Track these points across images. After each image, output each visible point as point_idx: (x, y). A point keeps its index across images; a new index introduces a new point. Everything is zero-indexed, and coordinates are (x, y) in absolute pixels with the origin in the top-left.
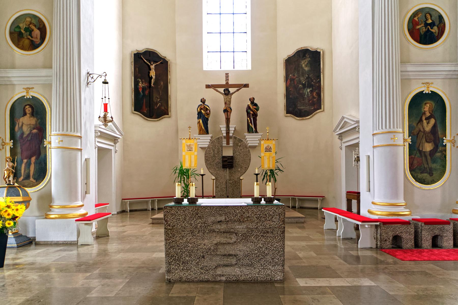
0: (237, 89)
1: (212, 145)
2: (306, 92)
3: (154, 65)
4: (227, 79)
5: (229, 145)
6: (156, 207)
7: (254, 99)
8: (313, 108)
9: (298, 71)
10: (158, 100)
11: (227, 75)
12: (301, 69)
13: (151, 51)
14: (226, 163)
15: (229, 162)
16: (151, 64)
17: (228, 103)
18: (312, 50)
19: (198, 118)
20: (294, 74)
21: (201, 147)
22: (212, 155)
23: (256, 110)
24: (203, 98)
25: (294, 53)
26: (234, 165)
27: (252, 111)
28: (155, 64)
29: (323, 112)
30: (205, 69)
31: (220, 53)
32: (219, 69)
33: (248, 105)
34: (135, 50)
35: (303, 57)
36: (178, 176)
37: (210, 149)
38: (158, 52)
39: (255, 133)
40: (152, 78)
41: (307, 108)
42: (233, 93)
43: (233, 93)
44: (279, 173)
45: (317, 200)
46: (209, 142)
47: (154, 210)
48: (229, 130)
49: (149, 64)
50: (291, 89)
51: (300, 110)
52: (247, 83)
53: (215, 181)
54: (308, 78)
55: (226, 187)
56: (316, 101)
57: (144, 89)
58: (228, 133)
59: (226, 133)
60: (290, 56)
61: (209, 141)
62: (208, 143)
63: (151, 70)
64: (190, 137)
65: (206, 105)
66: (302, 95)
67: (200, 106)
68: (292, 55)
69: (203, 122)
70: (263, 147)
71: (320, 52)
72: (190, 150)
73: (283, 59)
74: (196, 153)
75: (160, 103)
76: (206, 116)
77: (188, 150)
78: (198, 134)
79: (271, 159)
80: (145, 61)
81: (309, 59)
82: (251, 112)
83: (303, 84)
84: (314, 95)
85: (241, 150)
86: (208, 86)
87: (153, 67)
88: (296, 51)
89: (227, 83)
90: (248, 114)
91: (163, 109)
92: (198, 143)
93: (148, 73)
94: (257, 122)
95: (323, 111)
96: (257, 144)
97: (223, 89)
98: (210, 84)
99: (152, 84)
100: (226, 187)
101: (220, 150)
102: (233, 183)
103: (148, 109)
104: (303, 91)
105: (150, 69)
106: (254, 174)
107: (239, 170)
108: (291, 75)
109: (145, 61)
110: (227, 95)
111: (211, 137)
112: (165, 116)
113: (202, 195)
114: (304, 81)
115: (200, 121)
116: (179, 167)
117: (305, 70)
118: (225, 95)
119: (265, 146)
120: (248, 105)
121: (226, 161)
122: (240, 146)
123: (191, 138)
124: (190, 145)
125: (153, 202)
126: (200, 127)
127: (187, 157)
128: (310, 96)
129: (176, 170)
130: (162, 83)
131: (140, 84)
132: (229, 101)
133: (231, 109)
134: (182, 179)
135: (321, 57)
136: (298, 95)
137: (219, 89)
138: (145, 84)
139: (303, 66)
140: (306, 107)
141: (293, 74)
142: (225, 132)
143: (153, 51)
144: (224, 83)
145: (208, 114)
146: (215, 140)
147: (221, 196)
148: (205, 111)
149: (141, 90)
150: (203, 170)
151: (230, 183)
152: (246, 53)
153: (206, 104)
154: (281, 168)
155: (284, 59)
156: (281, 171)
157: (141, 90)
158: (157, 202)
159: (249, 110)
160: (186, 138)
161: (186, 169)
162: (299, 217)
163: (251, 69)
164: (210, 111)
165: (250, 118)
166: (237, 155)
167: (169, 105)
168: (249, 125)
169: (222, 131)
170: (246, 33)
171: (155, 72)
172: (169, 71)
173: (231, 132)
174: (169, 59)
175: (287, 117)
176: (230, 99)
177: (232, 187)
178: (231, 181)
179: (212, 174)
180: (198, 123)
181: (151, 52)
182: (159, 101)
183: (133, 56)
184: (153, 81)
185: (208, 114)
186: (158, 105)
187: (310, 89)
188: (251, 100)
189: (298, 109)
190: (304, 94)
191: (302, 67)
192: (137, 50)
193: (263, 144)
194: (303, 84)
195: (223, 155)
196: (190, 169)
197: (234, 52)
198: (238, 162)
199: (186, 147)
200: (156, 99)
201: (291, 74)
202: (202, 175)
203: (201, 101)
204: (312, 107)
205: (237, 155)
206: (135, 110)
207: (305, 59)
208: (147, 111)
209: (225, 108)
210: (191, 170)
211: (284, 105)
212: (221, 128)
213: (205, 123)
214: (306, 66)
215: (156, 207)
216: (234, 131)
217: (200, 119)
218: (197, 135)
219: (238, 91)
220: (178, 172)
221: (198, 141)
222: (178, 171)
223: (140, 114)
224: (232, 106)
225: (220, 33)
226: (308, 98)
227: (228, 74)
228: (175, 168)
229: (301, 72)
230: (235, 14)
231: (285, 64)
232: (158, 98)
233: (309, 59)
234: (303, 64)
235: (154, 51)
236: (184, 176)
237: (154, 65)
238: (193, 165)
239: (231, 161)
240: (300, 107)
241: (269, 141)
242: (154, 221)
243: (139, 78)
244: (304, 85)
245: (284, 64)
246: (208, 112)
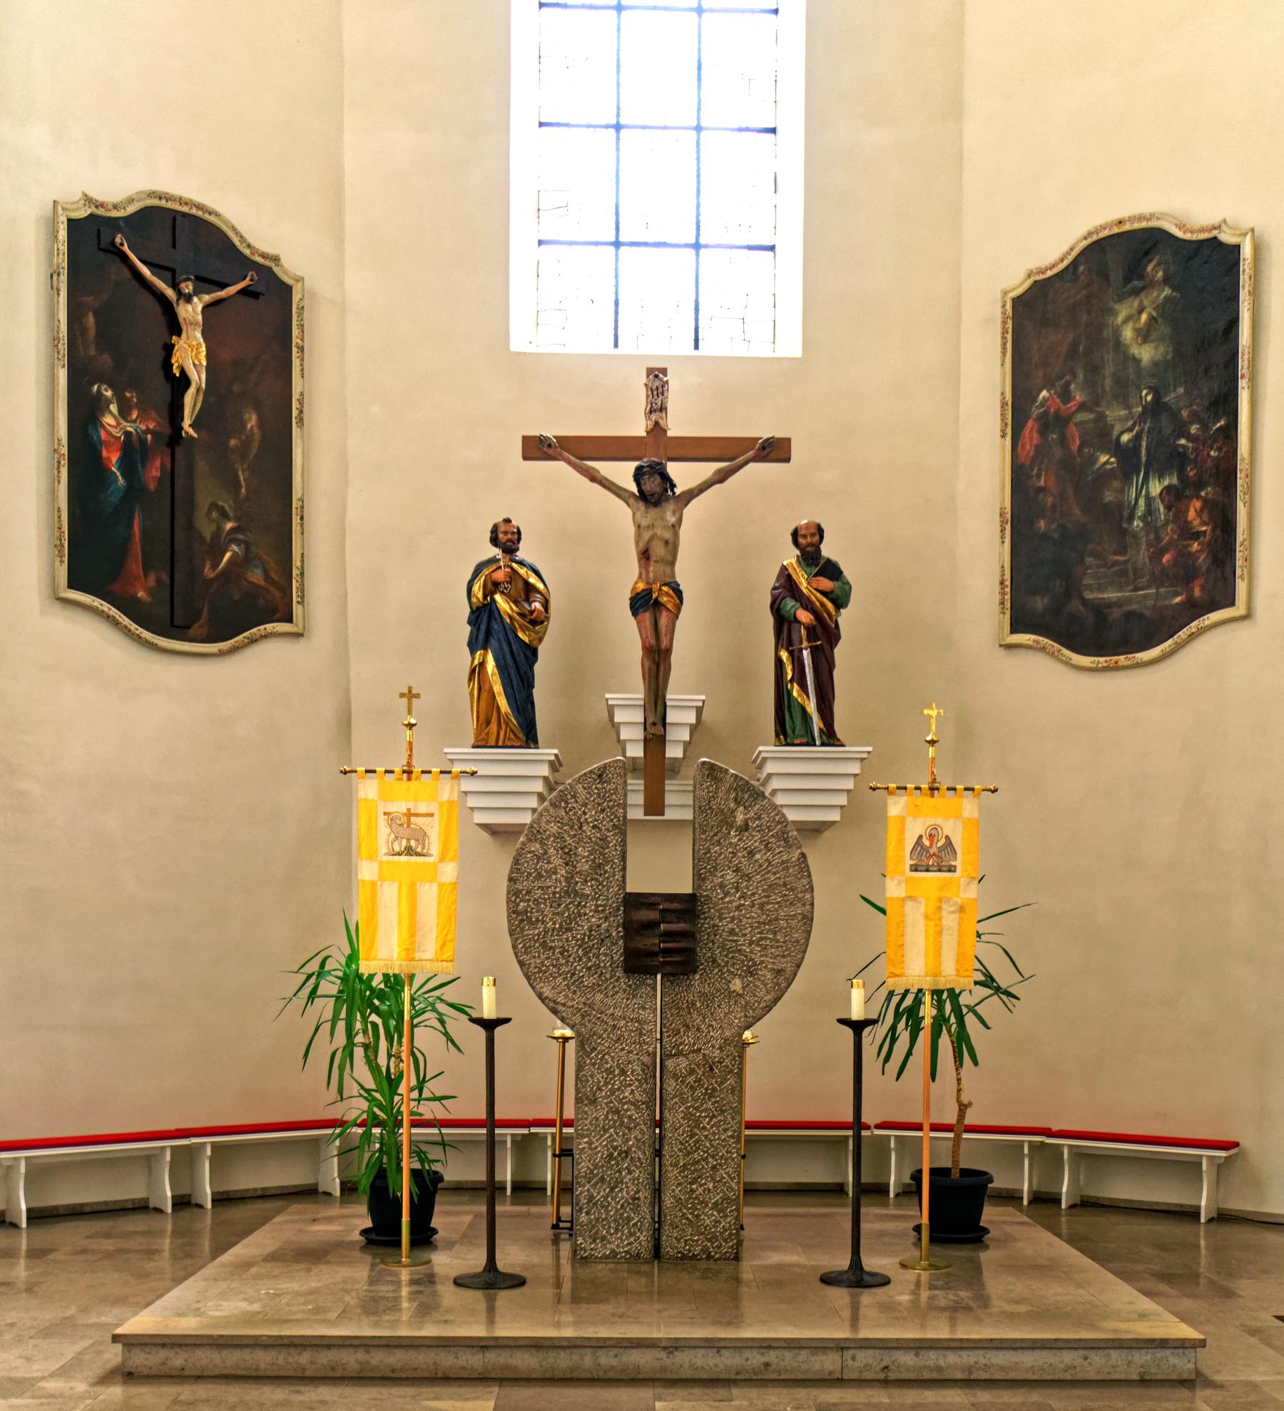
0: (719, 471)
1: (559, 821)
2: (1142, 502)
3: (198, 304)
4: (657, 407)
5: (663, 814)
6: (206, 1193)
7: (820, 531)
8: (1178, 599)
9: (1094, 369)
10: (229, 525)
11: (657, 380)
12: (1110, 357)
13: (185, 209)
14: (651, 942)
15: (668, 935)
16: (180, 294)
17: (658, 550)
18: (1188, 236)
19: (473, 645)
20: (1068, 384)
21: (486, 827)
22: (557, 882)
23: (834, 602)
24: (508, 521)
25: (1074, 254)
26: (702, 954)
27: (806, 608)
28: (207, 298)
29: (1246, 623)
30: (517, 345)
31: (612, 249)
32: (608, 348)
33: (784, 568)
34: (79, 195)
35: (1127, 280)
36: (328, 1014)
37: (542, 843)
38: (226, 222)
39: (823, 744)
40: (184, 381)
41: (1145, 597)
42: (691, 495)
43: (691, 495)
44: (992, 1007)
45: (1196, 1164)
46: (541, 797)
47: (196, 1210)
48: (664, 724)
49: (170, 293)
50: (1042, 483)
51: (1100, 610)
52: (779, 435)
53: (571, 1046)
54: (1156, 409)
55: (644, 1097)
56: (1201, 551)
57: (132, 450)
58: (655, 738)
59: (646, 741)
60: (1042, 271)
61: (539, 787)
62: (533, 802)
63: (179, 335)
64: (409, 764)
65: (521, 563)
66: (1117, 517)
67: (486, 572)
68: (1055, 271)
69: (500, 666)
70: (901, 840)
71: (1237, 248)
72: (409, 851)
73: (999, 295)
74: (449, 872)
75: (238, 542)
76: (520, 635)
77: (397, 849)
78: (472, 741)
79: (950, 920)
80: (145, 271)
81: (1167, 291)
82: (804, 616)
83: (1118, 449)
84: (1192, 514)
85: (751, 853)
86: (537, 448)
87: (192, 311)
88: (1085, 243)
89: (657, 430)
90: (783, 623)
91: (258, 586)
92: (472, 802)
93: (163, 354)
94: (836, 674)
95: (1247, 617)
96: (835, 816)
97: (632, 466)
98: (550, 432)
99: (186, 424)
100: (644, 1097)
101: (613, 851)
102: (692, 1072)
103: (159, 581)
104: (1121, 491)
105: (175, 327)
106: (841, 1021)
107: (737, 985)
108: (1044, 393)
109: (145, 271)
110: (657, 504)
111: (551, 763)
112: (269, 627)
113: (482, 1115)
114: (1130, 430)
115: (482, 664)
116: (336, 963)
117: (1137, 361)
118: (641, 505)
119: (916, 829)
120: (784, 568)
121: (651, 925)
122: (745, 827)
123: (417, 769)
124: (409, 814)
125: (185, 1162)
126: (483, 703)
127: (390, 895)
128: (1167, 523)
129: (321, 973)
130: (252, 421)
131: (108, 420)
132: (667, 542)
133: (679, 594)
134: (360, 1039)
135: (1244, 279)
136: (1084, 520)
137: (606, 468)
138: (143, 417)
139: (1128, 334)
140: (1136, 589)
141: (1059, 384)
142: (638, 734)
143: (194, 211)
144: (638, 428)
145: (534, 623)
146: (579, 788)
147: (610, 1156)
148: (516, 602)
149: (114, 460)
150: (493, 989)
151: (675, 1076)
152: (770, 254)
153: (520, 555)
154: (1004, 977)
155: (1005, 293)
156: (1004, 997)
157: (113, 459)
158: (212, 1159)
159: (790, 603)
160: (380, 769)
161: (386, 977)
162: (1163, 1344)
163: (797, 352)
164: (546, 605)
165: (791, 653)
166: (722, 886)
167: (296, 562)
168: (789, 693)
169: (616, 727)
170: (773, 131)
171: (204, 348)
172: (294, 350)
173: (672, 734)
174: (299, 273)
175: (1014, 651)
176: (675, 527)
177: (683, 1101)
178: (683, 1063)
179: (555, 1012)
180: (473, 671)
181: (179, 218)
182: (232, 530)
183: (63, 234)
184: (191, 402)
185: (534, 623)
186: (228, 555)
187: (1166, 482)
188: (801, 540)
189: (1084, 602)
190: (1126, 514)
191: (1118, 344)
192: (88, 200)
193: (902, 819)
194: (1118, 449)
195: (630, 888)
196: (411, 977)
197: (697, 246)
198: (732, 932)
199: (383, 830)
200: (214, 515)
201: (1048, 384)
202: (490, 1026)
203: (495, 541)
204: (1176, 594)
205: (722, 886)
206: (72, 585)
207: (1136, 292)
208: (150, 591)
209: (641, 586)
210: (416, 984)
211: (998, 579)
212: (611, 710)
213: (513, 672)
214: (1144, 335)
215: (206, 1193)
216: (694, 729)
217: (485, 648)
218: (462, 752)
219: (721, 481)
220: (334, 991)
221: (468, 785)
222: (330, 987)
223: (106, 607)
224: (683, 574)
225: (618, 127)
226: (1152, 536)
227: (664, 371)
228: (313, 967)
229: (1108, 370)
230: (712, 11)
231: (1010, 325)
232: (224, 515)
233: (1167, 291)
234: (1125, 322)
235: (200, 214)
236: (374, 1018)
237: (198, 304)
238: (429, 950)
239: (680, 926)
240: (1101, 589)
241: (938, 800)
242: (140, 1359)
243: (101, 380)
244: (1128, 457)
245: (1004, 323)
246: (537, 605)
